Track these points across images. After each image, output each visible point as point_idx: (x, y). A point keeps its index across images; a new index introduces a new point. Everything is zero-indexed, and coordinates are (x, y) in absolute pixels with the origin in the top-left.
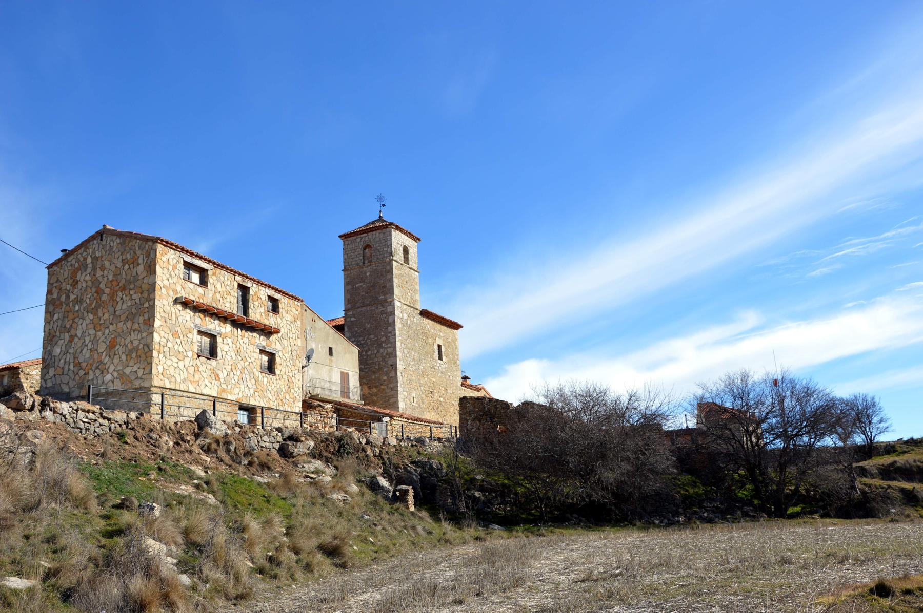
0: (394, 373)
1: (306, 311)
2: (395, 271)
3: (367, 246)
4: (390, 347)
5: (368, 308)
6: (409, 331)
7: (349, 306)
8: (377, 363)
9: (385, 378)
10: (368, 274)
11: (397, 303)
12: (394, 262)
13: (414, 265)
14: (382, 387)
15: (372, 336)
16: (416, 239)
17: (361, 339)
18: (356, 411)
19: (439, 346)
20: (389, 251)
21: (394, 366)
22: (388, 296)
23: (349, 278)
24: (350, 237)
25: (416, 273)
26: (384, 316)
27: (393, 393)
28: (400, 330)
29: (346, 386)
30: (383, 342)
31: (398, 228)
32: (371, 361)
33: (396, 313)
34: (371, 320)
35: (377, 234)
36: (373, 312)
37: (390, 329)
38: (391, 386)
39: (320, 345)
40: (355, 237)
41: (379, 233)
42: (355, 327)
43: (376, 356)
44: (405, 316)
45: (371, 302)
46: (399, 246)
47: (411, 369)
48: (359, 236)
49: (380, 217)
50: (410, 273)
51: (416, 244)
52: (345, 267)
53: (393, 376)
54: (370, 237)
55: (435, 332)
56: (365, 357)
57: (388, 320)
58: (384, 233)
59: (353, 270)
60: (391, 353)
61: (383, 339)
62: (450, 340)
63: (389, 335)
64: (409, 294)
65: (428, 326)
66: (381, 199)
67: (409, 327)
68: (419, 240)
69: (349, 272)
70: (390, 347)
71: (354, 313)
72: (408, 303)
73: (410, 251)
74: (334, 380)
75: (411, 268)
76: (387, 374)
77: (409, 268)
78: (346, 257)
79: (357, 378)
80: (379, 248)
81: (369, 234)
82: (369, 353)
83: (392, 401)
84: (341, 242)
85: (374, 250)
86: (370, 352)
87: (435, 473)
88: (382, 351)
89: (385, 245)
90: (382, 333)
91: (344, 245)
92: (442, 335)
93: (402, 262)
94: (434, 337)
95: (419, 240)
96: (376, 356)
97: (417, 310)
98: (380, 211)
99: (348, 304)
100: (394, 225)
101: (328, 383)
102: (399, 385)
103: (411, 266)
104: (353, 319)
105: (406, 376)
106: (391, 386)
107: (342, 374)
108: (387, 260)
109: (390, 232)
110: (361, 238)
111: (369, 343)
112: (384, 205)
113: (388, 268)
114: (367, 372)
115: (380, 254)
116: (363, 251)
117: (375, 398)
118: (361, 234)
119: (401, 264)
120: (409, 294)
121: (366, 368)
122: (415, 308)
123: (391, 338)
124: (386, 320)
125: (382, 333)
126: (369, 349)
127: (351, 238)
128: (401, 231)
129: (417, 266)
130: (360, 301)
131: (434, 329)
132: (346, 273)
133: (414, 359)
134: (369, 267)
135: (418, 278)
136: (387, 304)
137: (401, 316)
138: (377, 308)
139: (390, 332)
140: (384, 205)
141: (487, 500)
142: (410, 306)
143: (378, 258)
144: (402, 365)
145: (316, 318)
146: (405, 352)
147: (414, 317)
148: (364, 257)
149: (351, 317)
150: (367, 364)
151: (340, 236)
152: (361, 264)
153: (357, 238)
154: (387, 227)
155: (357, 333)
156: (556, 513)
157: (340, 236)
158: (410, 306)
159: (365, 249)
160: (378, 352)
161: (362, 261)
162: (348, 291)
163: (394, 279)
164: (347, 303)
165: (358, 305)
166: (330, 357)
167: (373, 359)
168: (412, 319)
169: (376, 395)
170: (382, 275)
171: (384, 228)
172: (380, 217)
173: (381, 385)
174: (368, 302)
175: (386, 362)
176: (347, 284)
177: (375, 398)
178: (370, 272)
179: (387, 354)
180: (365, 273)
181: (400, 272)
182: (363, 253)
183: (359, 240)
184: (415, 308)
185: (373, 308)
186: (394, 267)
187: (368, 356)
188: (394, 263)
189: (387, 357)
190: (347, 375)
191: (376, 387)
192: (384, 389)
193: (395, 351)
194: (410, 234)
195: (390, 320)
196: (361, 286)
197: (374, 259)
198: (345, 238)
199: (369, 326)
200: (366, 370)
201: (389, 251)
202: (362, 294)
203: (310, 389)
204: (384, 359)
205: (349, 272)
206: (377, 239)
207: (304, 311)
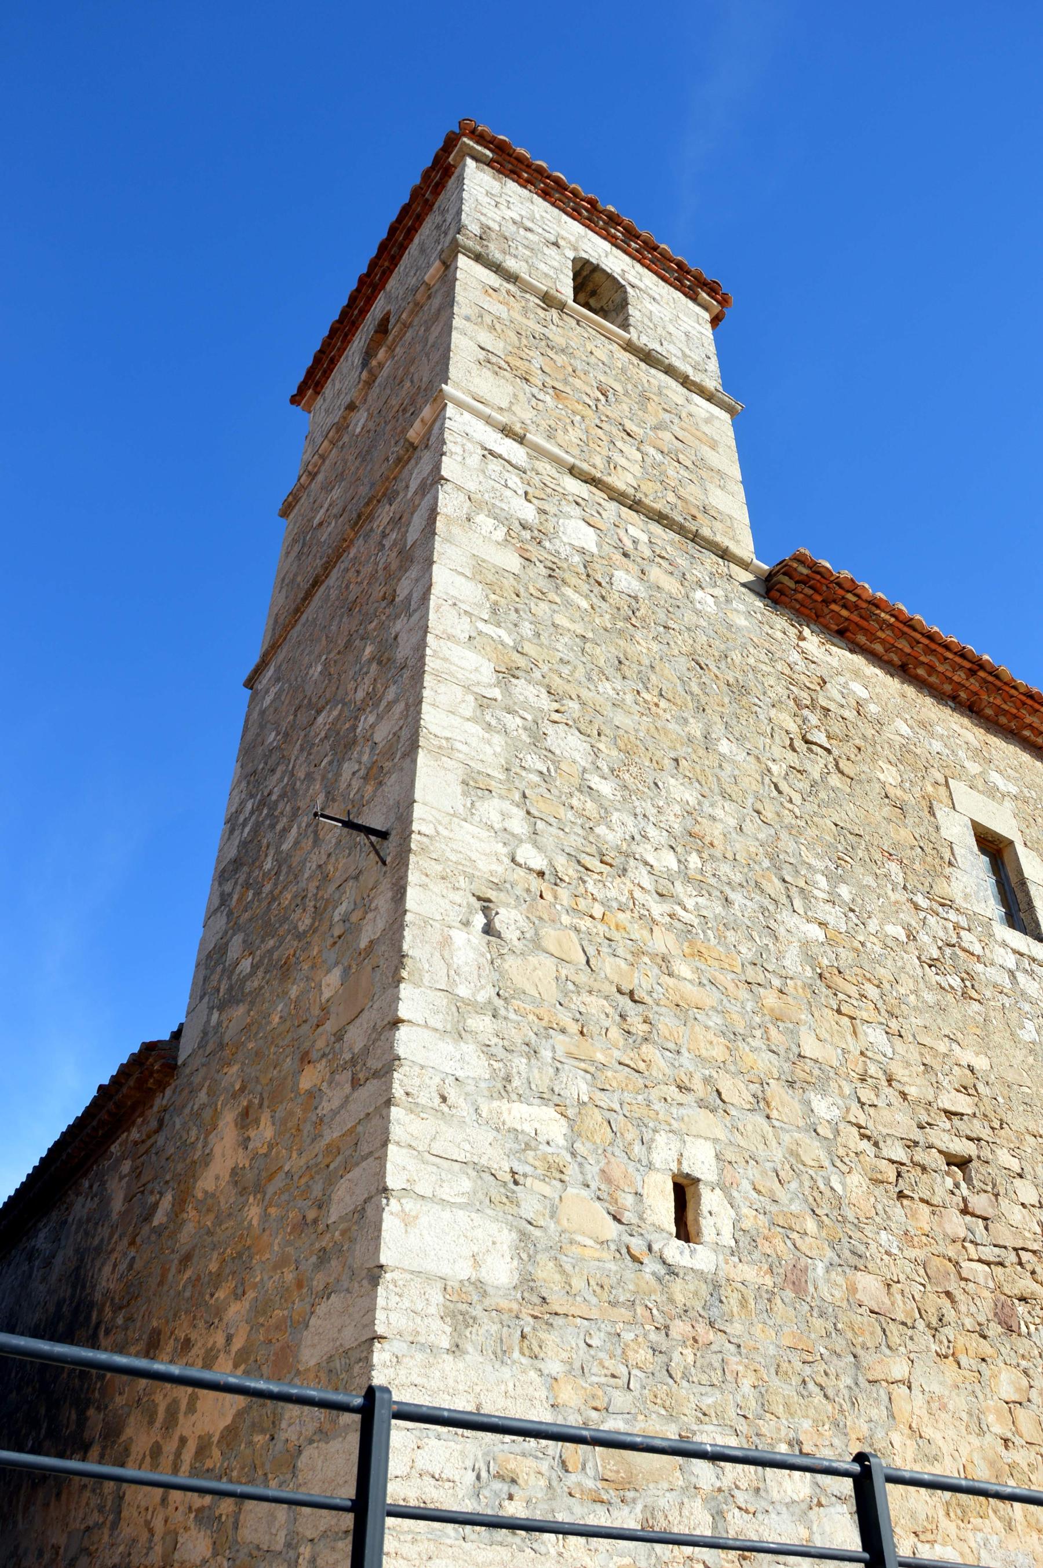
75: (648, 357)
77: (629, 347)
103: (646, 341)
119: (548, 300)
128: (545, 195)
194: (631, 234)
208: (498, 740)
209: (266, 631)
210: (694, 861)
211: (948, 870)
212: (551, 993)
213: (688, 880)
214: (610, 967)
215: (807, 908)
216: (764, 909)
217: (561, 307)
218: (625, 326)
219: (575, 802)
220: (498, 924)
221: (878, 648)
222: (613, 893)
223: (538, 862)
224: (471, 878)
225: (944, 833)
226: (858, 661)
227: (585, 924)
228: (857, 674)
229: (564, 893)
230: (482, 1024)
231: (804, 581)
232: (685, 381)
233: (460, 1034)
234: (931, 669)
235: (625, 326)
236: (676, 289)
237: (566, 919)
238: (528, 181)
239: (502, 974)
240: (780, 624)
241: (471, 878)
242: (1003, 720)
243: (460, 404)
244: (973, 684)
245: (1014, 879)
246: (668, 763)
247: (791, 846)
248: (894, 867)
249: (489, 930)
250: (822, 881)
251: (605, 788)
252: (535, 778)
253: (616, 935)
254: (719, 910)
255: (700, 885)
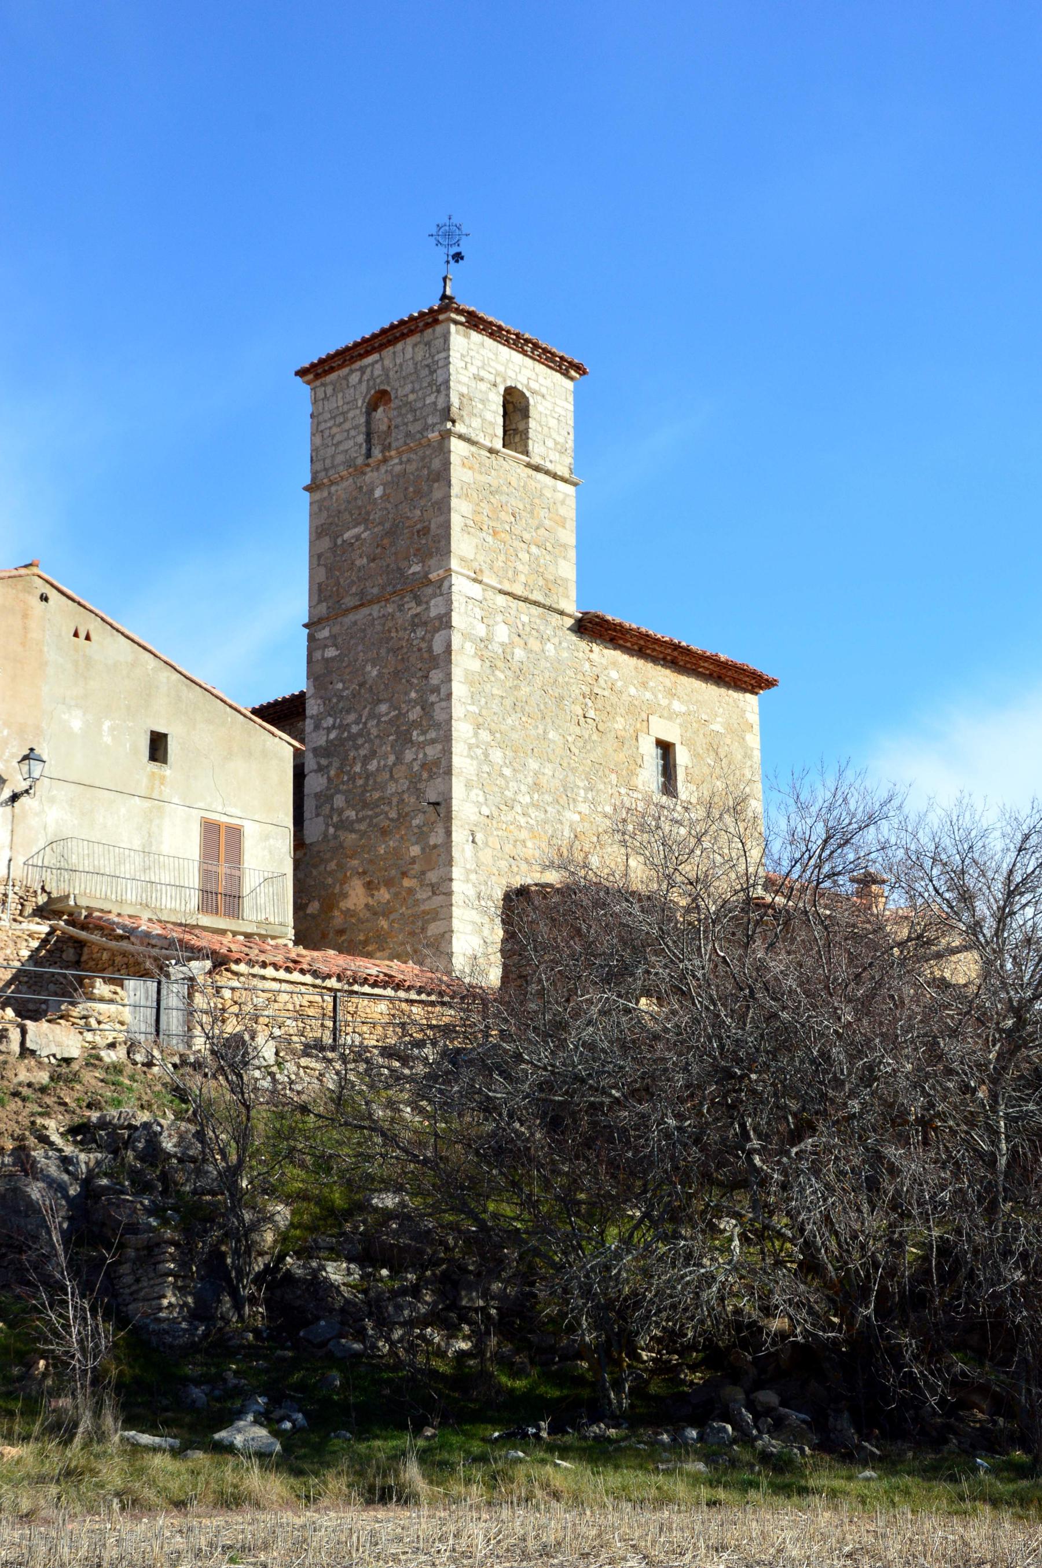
0: (441, 831)
1: (44, 598)
2: (459, 475)
3: (380, 398)
4: (433, 742)
5: (375, 610)
6: (517, 687)
7: (323, 608)
8: (395, 800)
9: (415, 850)
10: (378, 493)
11: (461, 587)
12: (453, 439)
13: (554, 456)
14: (407, 883)
15: (383, 708)
16: (566, 366)
17: (351, 717)
18: (124, 945)
19: (666, 748)
20: (441, 404)
21: (442, 808)
22: (432, 562)
23: (325, 514)
24: (332, 370)
25: (560, 485)
26: (420, 632)
27: (438, 900)
28: (472, 680)
29: (223, 869)
30: (415, 724)
31: (475, 322)
32: (376, 795)
33: (456, 619)
34: (383, 651)
35: (407, 350)
36: (390, 624)
37: (435, 677)
38: (432, 877)
39: (107, 725)
40: (345, 371)
41: (415, 345)
42: (335, 677)
43: (392, 776)
44: (502, 633)
45: (383, 588)
46: (483, 386)
47: (522, 820)
48: (357, 365)
49: (444, 297)
50: (532, 484)
51: (569, 385)
52: (314, 479)
53: (440, 841)
54: (387, 362)
55: (648, 695)
56: (360, 782)
57: (430, 650)
58: (428, 344)
59: (337, 483)
60: (437, 763)
61: (415, 714)
62: (716, 727)
63: (433, 698)
64: (524, 556)
65: (614, 674)
66: (449, 235)
67: (519, 674)
68: (579, 368)
69: (325, 494)
70: (433, 742)
71: (336, 629)
72: (518, 590)
73: (538, 408)
74: (165, 849)
75: (537, 468)
76: (421, 836)
77: (528, 465)
78: (318, 441)
79: (283, 844)
80: (412, 397)
81: (384, 353)
82: (373, 766)
83: (433, 929)
84: (303, 390)
85: (399, 407)
86: (375, 762)
87: (164, 1177)
88: (409, 755)
89: (430, 385)
90: (413, 695)
91: (315, 402)
92: (677, 706)
93: (498, 444)
94: (642, 714)
95: (579, 368)
96: (392, 776)
97: (562, 613)
98: (445, 279)
99: (320, 601)
100: (459, 311)
101: (138, 859)
102: (457, 872)
103: (536, 460)
104: (331, 652)
105: (493, 841)
106: (432, 877)
107: (211, 830)
108: (433, 436)
109: (446, 337)
110: (362, 370)
111: (374, 732)
112: (458, 257)
113: (436, 464)
114: (363, 834)
115: (415, 420)
116: (368, 414)
117: (384, 923)
118: (362, 356)
119: (491, 451)
120: (524, 556)
121: (363, 819)
122: (550, 608)
123: (437, 707)
124: (424, 645)
125: (413, 695)
126: (373, 754)
127: (333, 376)
128: (491, 335)
129: (569, 460)
130: (354, 590)
131: (644, 684)
132: (318, 496)
133: (536, 786)
134: (383, 469)
135: (572, 503)
136: (429, 591)
137: (481, 631)
138: (400, 608)
139: (436, 690)
140: (458, 257)
141: (368, 1303)
142: (526, 600)
143: (408, 434)
144: (478, 804)
145: (93, 626)
146: (497, 756)
147: (542, 639)
148: (369, 435)
149: (326, 646)
150: (365, 805)
151: (301, 373)
152: (360, 461)
153: (352, 371)
154: (436, 321)
155: (341, 698)
156: (472, 1362)
157: (301, 373)
158: (526, 600)
159: (372, 407)
160: (399, 760)
161: (364, 451)
162: (319, 556)
163: (454, 502)
164: (316, 598)
165: (349, 601)
166: (154, 767)
167: (383, 788)
168: (534, 644)
169: (386, 911)
170: (418, 492)
171: (428, 325)
172: (444, 297)
173: (404, 874)
174: (375, 591)
175: (419, 793)
176: (318, 532)
177: (384, 923)
178: (384, 485)
179: (423, 766)
180: (371, 491)
181: (484, 479)
182: (368, 423)
183: (354, 378)
184: (550, 608)
185: (390, 609)
186: (453, 458)
187: (368, 776)
188: (457, 446)
189: (425, 775)
190: (235, 834)
191: (389, 883)
192: (411, 891)
193: (448, 752)
194: (536, 346)
195: (438, 648)
196: (358, 537)
197: (397, 439)
198: (318, 376)
199: (375, 673)
200: (363, 827)
201: (441, 404)
202: (358, 563)
203: (47, 875)
204: (415, 787)
205: (325, 494)
206: (410, 367)
207: (35, 601)
208: (475, 762)
209: (621, 1494)
210: (536, 796)
211: (638, 769)
212: (490, 861)
213: (533, 805)
214: (508, 848)
215: (575, 806)
216: (559, 811)
217: (497, 452)
218: (527, 453)
219: (498, 782)
220: (476, 840)
221: (629, 645)
222: (509, 818)
223: (487, 813)
224: (468, 824)
225: (641, 750)
226: (617, 655)
227: (500, 833)
228: (614, 663)
229: (494, 822)
230: (473, 876)
231: (597, 624)
232: (555, 476)
233: (468, 881)
234: (654, 650)
235: (527, 453)
236: (556, 371)
237: (495, 833)
238: (483, 330)
239: (477, 857)
240: (583, 645)
241: (468, 824)
242: (689, 666)
243: (457, 573)
244: (676, 653)
245: (672, 762)
246: (530, 752)
247: (572, 778)
248: (613, 777)
249: (473, 842)
250: (582, 792)
251: (507, 772)
252: (486, 775)
253: (509, 835)
254: (543, 816)
255: (536, 806)
